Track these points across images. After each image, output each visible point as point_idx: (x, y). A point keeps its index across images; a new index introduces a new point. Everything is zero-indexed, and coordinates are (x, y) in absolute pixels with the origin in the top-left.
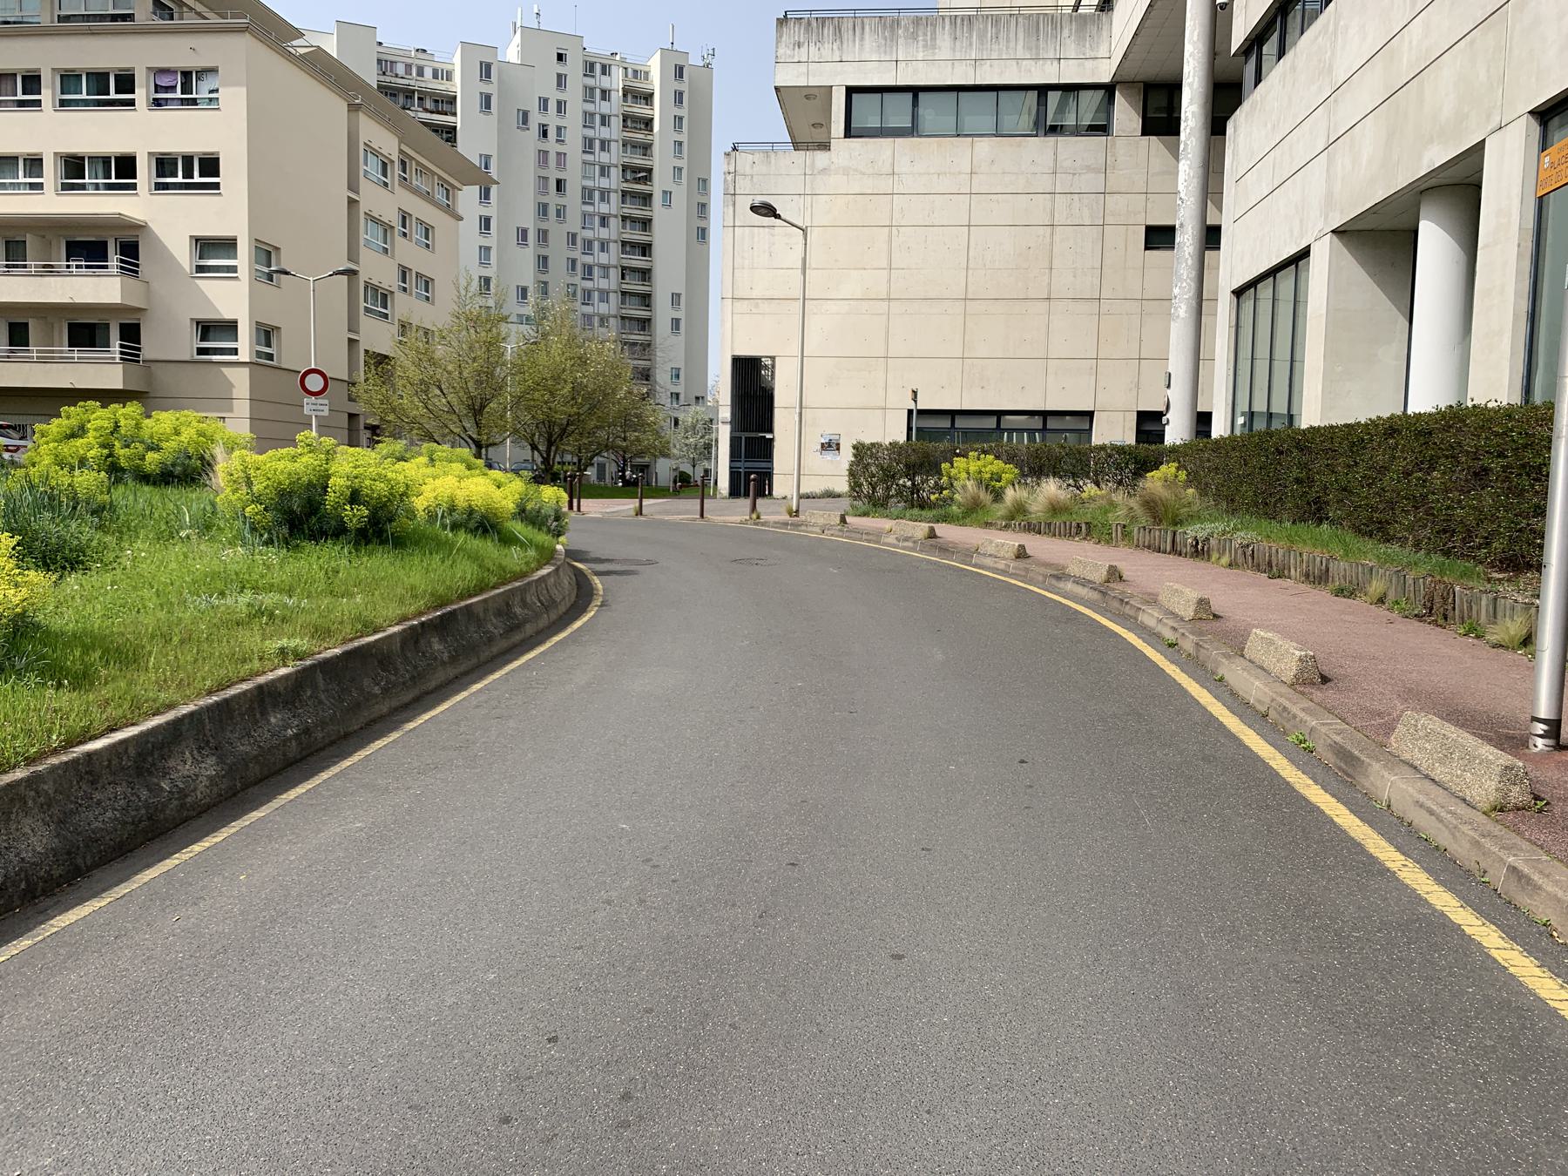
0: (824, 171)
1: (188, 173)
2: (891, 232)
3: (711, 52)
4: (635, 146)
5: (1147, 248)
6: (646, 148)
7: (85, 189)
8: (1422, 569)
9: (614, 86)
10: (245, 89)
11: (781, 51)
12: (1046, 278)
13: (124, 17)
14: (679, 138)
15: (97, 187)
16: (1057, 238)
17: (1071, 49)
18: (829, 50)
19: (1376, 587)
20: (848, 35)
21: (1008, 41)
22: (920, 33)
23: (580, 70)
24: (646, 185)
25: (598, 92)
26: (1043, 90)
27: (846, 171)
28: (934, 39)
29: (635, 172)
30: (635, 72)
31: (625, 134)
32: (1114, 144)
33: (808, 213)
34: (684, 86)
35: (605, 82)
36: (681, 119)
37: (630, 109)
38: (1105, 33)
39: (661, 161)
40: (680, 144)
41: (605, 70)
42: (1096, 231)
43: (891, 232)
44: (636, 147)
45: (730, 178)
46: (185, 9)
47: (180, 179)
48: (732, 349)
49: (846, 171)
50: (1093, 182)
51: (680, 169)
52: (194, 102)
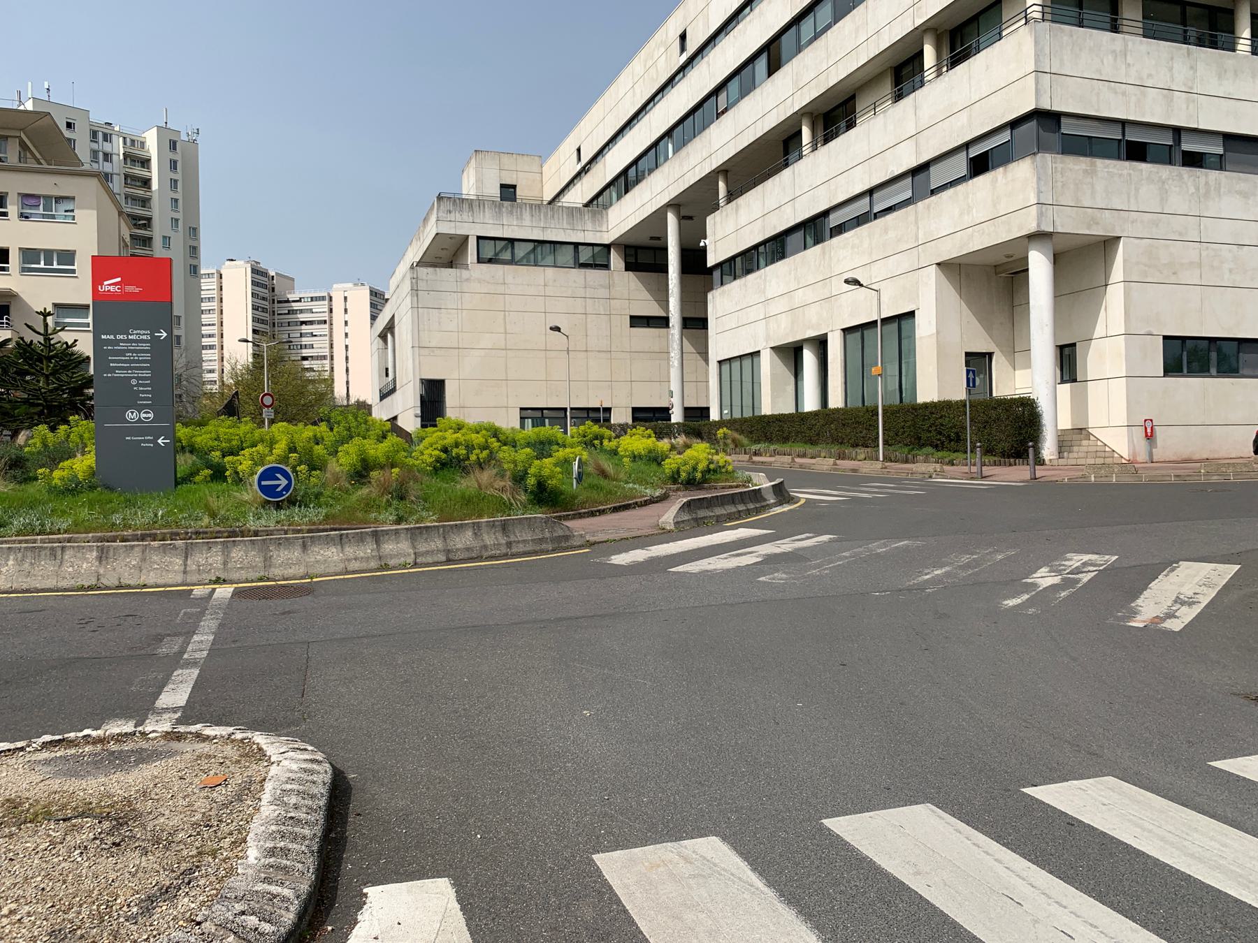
0: (467, 280)
1: (49, 261)
2: (505, 315)
3: (196, 131)
4: (135, 199)
5: (631, 327)
6: (145, 202)
7: (5, 271)
8: (835, 449)
9: (115, 151)
10: (95, 212)
11: (440, 214)
12: (585, 340)
14: (175, 196)
16: (588, 320)
17: (589, 226)
18: (466, 216)
19: (823, 454)
20: (476, 209)
21: (559, 219)
22: (514, 211)
23: (88, 137)
24: (146, 230)
25: (101, 155)
26: (576, 245)
27: (480, 281)
28: (521, 215)
30: (133, 141)
31: (127, 189)
32: (612, 274)
33: (460, 302)
34: (177, 157)
35: (107, 147)
36: (176, 181)
37: (131, 171)
38: (605, 220)
39: (159, 212)
40: (176, 200)
41: (107, 138)
42: (607, 318)
43: (505, 315)
44: (135, 200)
45: (414, 281)
46: (28, 155)
47: (42, 265)
48: (420, 375)
49: (480, 281)
50: (603, 293)
51: (177, 220)
52: (53, 217)
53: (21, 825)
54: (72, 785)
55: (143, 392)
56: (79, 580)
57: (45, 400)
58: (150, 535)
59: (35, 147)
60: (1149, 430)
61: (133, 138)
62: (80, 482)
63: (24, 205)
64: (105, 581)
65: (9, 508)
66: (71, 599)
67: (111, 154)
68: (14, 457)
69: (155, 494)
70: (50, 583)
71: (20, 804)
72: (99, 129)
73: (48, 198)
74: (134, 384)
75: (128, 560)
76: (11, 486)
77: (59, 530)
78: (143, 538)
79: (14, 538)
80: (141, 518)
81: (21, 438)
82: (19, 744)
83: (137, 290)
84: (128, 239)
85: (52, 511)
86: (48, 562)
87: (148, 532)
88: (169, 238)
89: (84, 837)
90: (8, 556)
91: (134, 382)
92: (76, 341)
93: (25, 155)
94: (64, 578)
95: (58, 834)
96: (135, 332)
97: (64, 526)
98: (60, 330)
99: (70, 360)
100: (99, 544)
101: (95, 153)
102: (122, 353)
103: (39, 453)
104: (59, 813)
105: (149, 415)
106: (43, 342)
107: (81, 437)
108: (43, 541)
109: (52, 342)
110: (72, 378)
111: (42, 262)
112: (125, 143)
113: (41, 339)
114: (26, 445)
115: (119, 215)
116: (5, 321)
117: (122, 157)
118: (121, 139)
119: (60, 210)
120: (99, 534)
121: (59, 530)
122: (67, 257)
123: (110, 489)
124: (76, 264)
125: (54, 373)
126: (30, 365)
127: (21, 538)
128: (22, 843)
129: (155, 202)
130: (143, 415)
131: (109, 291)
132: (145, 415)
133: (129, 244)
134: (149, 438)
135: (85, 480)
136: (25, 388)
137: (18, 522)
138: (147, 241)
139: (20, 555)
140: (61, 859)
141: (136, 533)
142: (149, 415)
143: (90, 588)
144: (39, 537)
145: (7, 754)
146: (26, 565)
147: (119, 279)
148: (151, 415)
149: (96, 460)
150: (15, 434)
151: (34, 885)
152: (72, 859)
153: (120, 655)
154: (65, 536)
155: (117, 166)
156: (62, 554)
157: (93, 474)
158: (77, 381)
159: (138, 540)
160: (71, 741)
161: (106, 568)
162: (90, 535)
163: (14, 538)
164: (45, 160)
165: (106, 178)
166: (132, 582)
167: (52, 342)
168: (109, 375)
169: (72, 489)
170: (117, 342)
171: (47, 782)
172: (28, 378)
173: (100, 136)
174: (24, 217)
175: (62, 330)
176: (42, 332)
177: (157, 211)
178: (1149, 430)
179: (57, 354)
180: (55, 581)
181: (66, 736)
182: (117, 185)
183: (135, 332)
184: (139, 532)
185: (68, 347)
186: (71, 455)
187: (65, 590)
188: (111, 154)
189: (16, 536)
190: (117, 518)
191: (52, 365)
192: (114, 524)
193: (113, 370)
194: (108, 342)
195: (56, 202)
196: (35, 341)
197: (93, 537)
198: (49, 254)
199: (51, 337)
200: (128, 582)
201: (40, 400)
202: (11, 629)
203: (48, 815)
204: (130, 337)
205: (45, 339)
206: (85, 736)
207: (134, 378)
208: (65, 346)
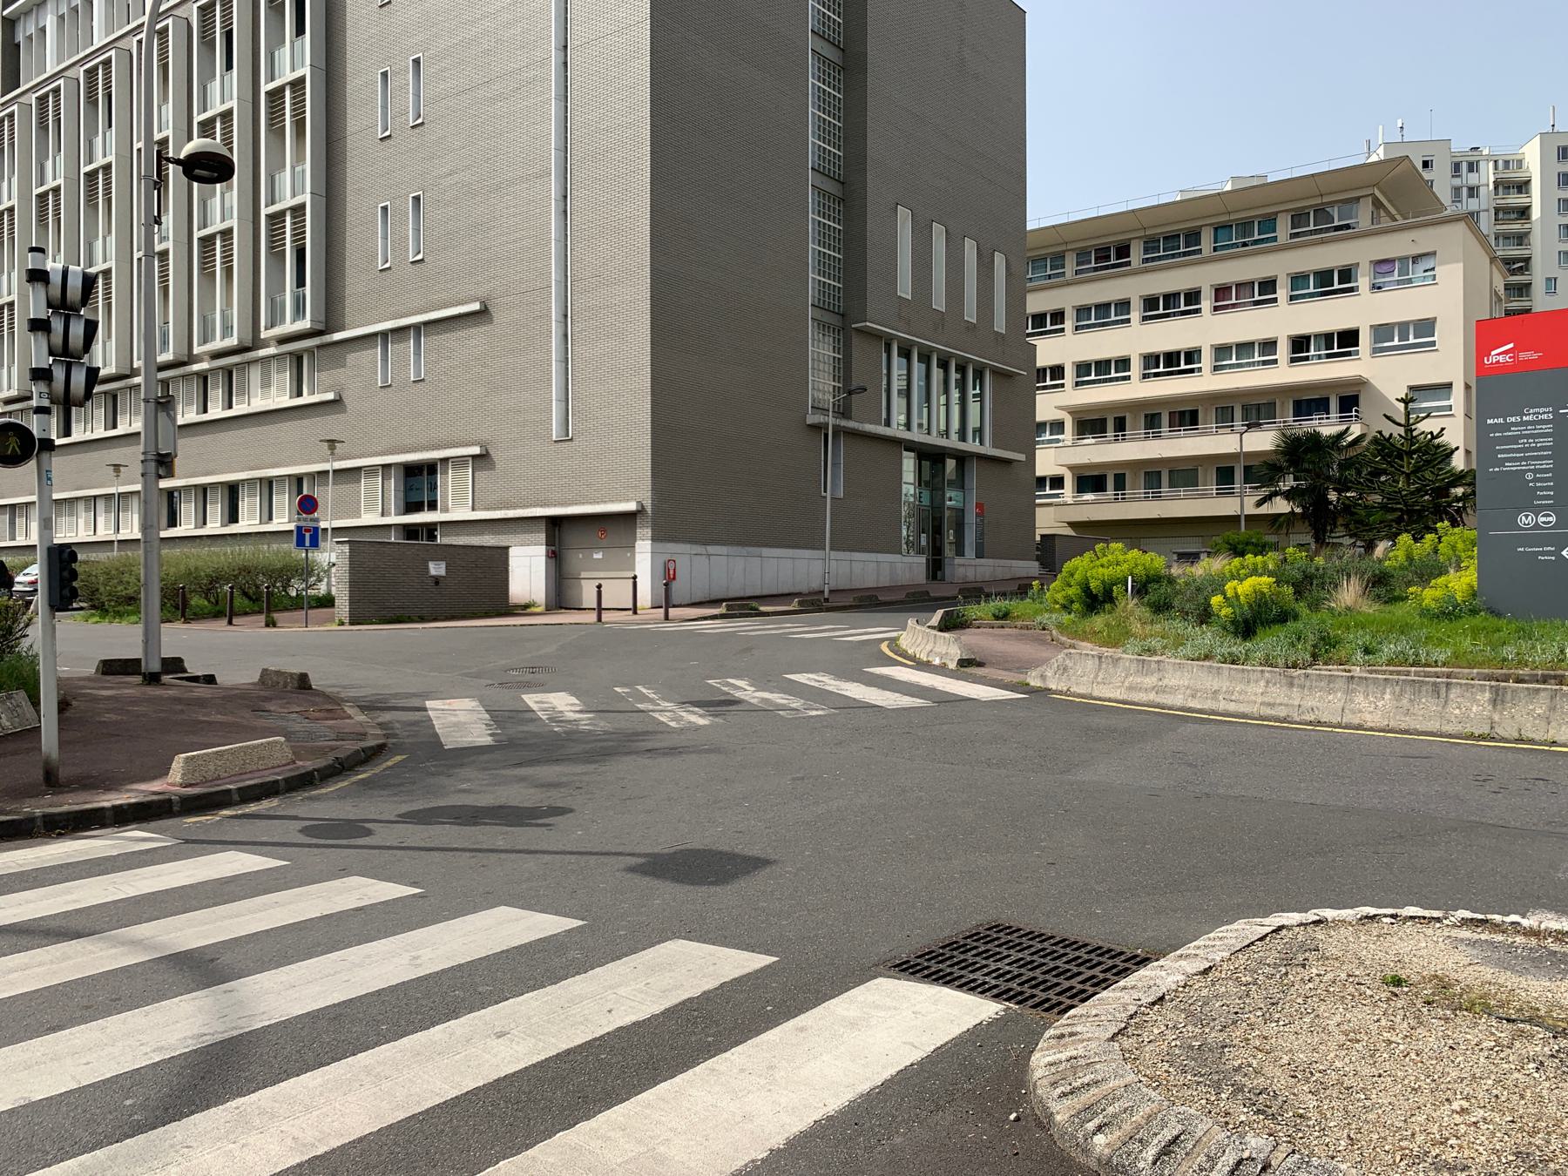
1: (1404, 337)
6: (1521, 238)
10: (1462, 264)
13: (1348, 227)
15: (1319, 357)
24: (1523, 274)
29: (1509, 264)
31: (1498, 227)
35: (1473, 179)
37: (1503, 201)
41: (1472, 167)
44: (1509, 238)
46: (1382, 213)
47: (1396, 342)
52: (1410, 281)
53: (1455, 1010)
54: (1509, 979)
55: (1542, 488)
56: (1468, 725)
57: (1406, 505)
58: (1555, 677)
59: (1389, 201)
60: (671, 572)
61: (1507, 158)
62: (1459, 605)
63: (1377, 274)
64: (1500, 731)
65: (1377, 632)
66: (1460, 748)
67: (1478, 187)
68: (1377, 572)
69: (1558, 622)
70: (1433, 726)
71: (1451, 986)
72: (1460, 159)
73: (1404, 259)
74: (1530, 478)
75: (1531, 707)
76: (1376, 606)
77: (1436, 662)
78: (1545, 679)
79: (1384, 668)
80: (1542, 653)
81: (1381, 548)
82: (1436, 914)
83: (1535, 356)
84: (1501, 291)
85: (1426, 638)
86: (1429, 699)
87: (1552, 673)
88: (1555, 279)
89: (1537, 1049)
90: (1385, 689)
91: (1529, 476)
92: (1443, 429)
93: (1379, 214)
94: (1449, 721)
95: (1503, 1035)
96: (1531, 411)
97: (1442, 657)
98: (1424, 418)
99: (1436, 454)
100: (1493, 683)
101: (1457, 191)
102: (1514, 440)
103: (1402, 568)
104: (1501, 1011)
105: (1550, 519)
106: (1403, 435)
107: (1454, 548)
108: (1416, 674)
109: (1415, 434)
110: (1438, 475)
111: (1396, 339)
112: (1496, 168)
113: (1402, 431)
114: (1387, 558)
115: (1491, 263)
116: (1354, 413)
117: (1491, 187)
118: (1491, 164)
119: (1417, 272)
120: (1486, 671)
121: (1436, 662)
122: (1426, 327)
123: (1496, 613)
124: (1436, 334)
125: (1417, 470)
126: (1389, 463)
127: (1391, 668)
128: (1460, 1032)
129: (1536, 239)
130: (1541, 519)
131: (1498, 362)
132: (1544, 519)
133: (1503, 297)
134: (1549, 548)
135: (1465, 602)
136: (1383, 491)
137: (1388, 649)
138: (1523, 289)
139: (1397, 689)
140: (1513, 1067)
141: (1535, 672)
142: (1550, 519)
143: (1482, 737)
144: (1413, 669)
145: (1422, 921)
146: (1405, 702)
147: (1511, 345)
148: (1553, 519)
149: (1478, 577)
150: (1370, 547)
151: (1486, 1087)
152: (1528, 1072)
153: (1533, 828)
154: (1444, 669)
155: (1485, 201)
156: (1447, 692)
157: (1474, 595)
158: (1444, 479)
159: (1538, 682)
160: (1497, 925)
161: (1501, 714)
162: (1475, 671)
163: (1384, 668)
164: (1401, 215)
165: (1471, 218)
166: (1537, 737)
167: (1415, 434)
168: (1497, 469)
169: (1448, 613)
170: (1507, 426)
171: (1476, 968)
172: (1383, 479)
173: (1464, 167)
174: (1376, 288)
175: (1428, 416)
176: (1403, 422)
177: (1539, 250)
178: (671, 572)
179: (1419, 448)
180: (1438, 724)
181: (1489, 917)
182: (1486, 223)
183: (1531, 411)
184: (1540, 672)
185: (1434, 437)
186: (1442, 571)
187: (1450, 736)
188: (1478, 187)
189: (1387, 665)
190: (1509, 652)
191: (1413, 462)
192: (1505, 660)
193: (1502, 462)
194: (1495, 427)
195: (1414, 262)
196: (1395, 435)
197: (1478, 673)
198: (1404, 327)
199: (1413, 427)
200: (1531, 736)
201: (1400, 503)
202: (1395, 775)
203: (1488, 1011)
204: (1525, 418)
205: (1406, 432)
206: (1513, 923)
207: (1530, 470)
208: (1429, 436)
